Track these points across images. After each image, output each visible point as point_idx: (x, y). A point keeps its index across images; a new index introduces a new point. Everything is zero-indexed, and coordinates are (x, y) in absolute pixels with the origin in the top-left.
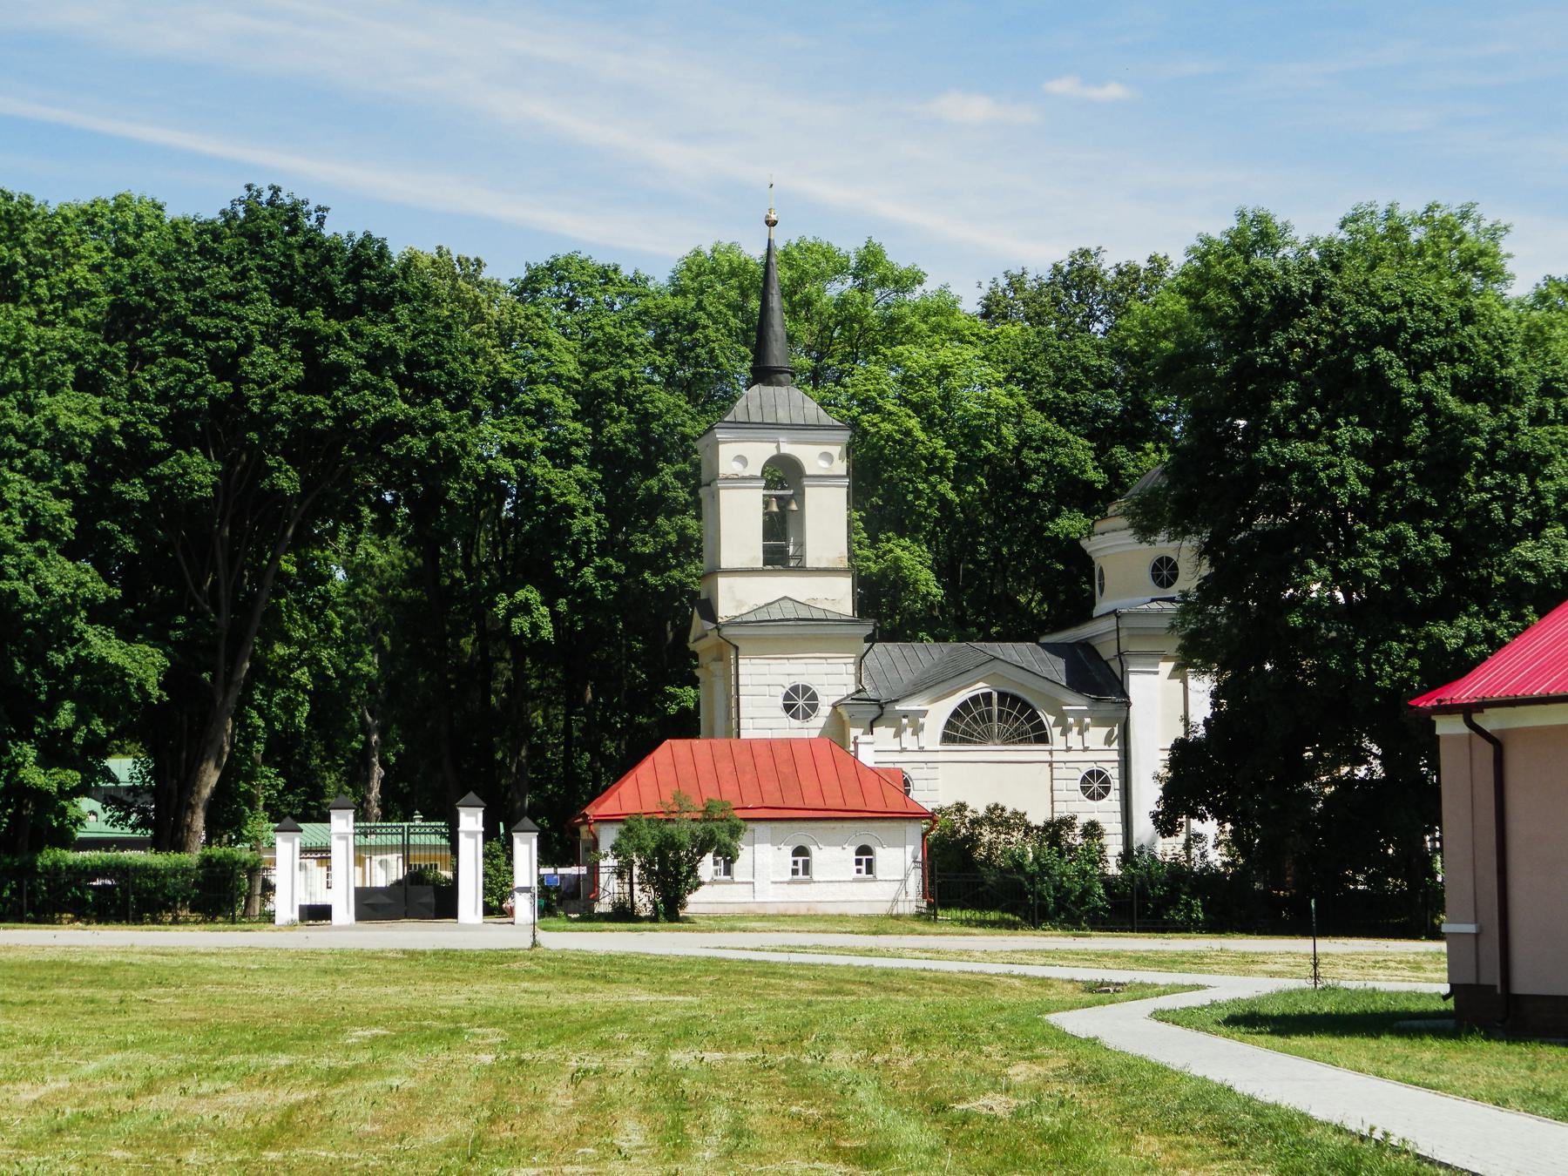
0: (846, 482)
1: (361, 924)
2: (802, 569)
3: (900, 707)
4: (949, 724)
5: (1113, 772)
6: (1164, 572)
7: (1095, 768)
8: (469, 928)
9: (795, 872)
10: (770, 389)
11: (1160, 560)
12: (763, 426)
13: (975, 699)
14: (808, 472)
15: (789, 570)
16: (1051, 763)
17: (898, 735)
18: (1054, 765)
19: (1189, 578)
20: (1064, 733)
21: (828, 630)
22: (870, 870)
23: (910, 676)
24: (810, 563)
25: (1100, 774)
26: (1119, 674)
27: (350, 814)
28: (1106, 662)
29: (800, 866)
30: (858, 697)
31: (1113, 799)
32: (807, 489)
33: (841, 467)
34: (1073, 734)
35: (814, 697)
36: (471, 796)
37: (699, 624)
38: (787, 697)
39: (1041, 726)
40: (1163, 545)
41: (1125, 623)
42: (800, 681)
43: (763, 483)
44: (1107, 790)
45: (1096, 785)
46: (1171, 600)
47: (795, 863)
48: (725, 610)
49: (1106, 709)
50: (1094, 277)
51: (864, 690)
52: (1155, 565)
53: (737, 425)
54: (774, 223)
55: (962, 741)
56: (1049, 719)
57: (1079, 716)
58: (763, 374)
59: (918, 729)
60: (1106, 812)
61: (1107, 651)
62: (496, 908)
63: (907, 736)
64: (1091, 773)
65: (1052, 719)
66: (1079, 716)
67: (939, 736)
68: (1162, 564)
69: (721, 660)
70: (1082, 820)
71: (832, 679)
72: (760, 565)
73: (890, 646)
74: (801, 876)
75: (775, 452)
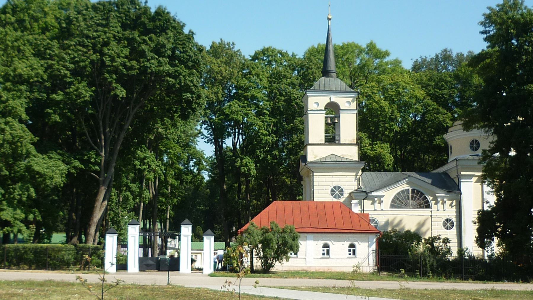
0: (356, 112)
1: (143, 273)
2: (340, 144)
3: (374, 194)
4: (393, 201)
5: (454, 219)
6: (475, 145)
7: (448, 218)
8: (184, 275)
9: (324, 254)
10: (328, 79)
11: (473, 141)
12: (325, 91)
13: (403, 191)
14: (341, 108)
15: (336, 144)
16: (431, 216)
17: (373, 203)
18: (433, 216)
19: (485, 145)
20: (437, 203)
21: (348, 166)
22: (354, 253)
23: (379, 183)
24: (342, 142)
25: (450, 220)
26: (457, 184)
27: (213, 238)
28: (453, 179)
29: (325, 252)
30: (358, 190)
31: (454, 230)
32: (341, 114)
33: (354, 106)
34: (440, 205)
35: (342, 190)
36: (187, 221)
37: (302, 164)
38: (332, 190)
39: (428, 202)
40: (476, 134)
41: (459, 163)
42: (337, 184)
43: (325, 112)
44: (453, 226)
45: (448, 224)
46: (477, 155)
47: (324, 251)
48: (310, 159)
49: (453, 195)
50: (450, 56)
51: (361, 188)
52: (471, 143)
53: (315, 91)
54: (330, 19)
55: (398, 207)
56: (430, 198)
57: (443, 198)
58: (326, 73)
59: (380, 202)
60: (452, 234)
61: (453, 175)
62: (122, 266)
63: (377, 205)
64: (447, 220)
65: (431, 198)
66: (443, 198)
67: (389, 205)
68: (472, 145)
69: (308, 177)
70: (443, 237)
71: (349, 184)
72: (323, 142)
73: (372, 173)
74: (326, 256)
75: (329, 101)
